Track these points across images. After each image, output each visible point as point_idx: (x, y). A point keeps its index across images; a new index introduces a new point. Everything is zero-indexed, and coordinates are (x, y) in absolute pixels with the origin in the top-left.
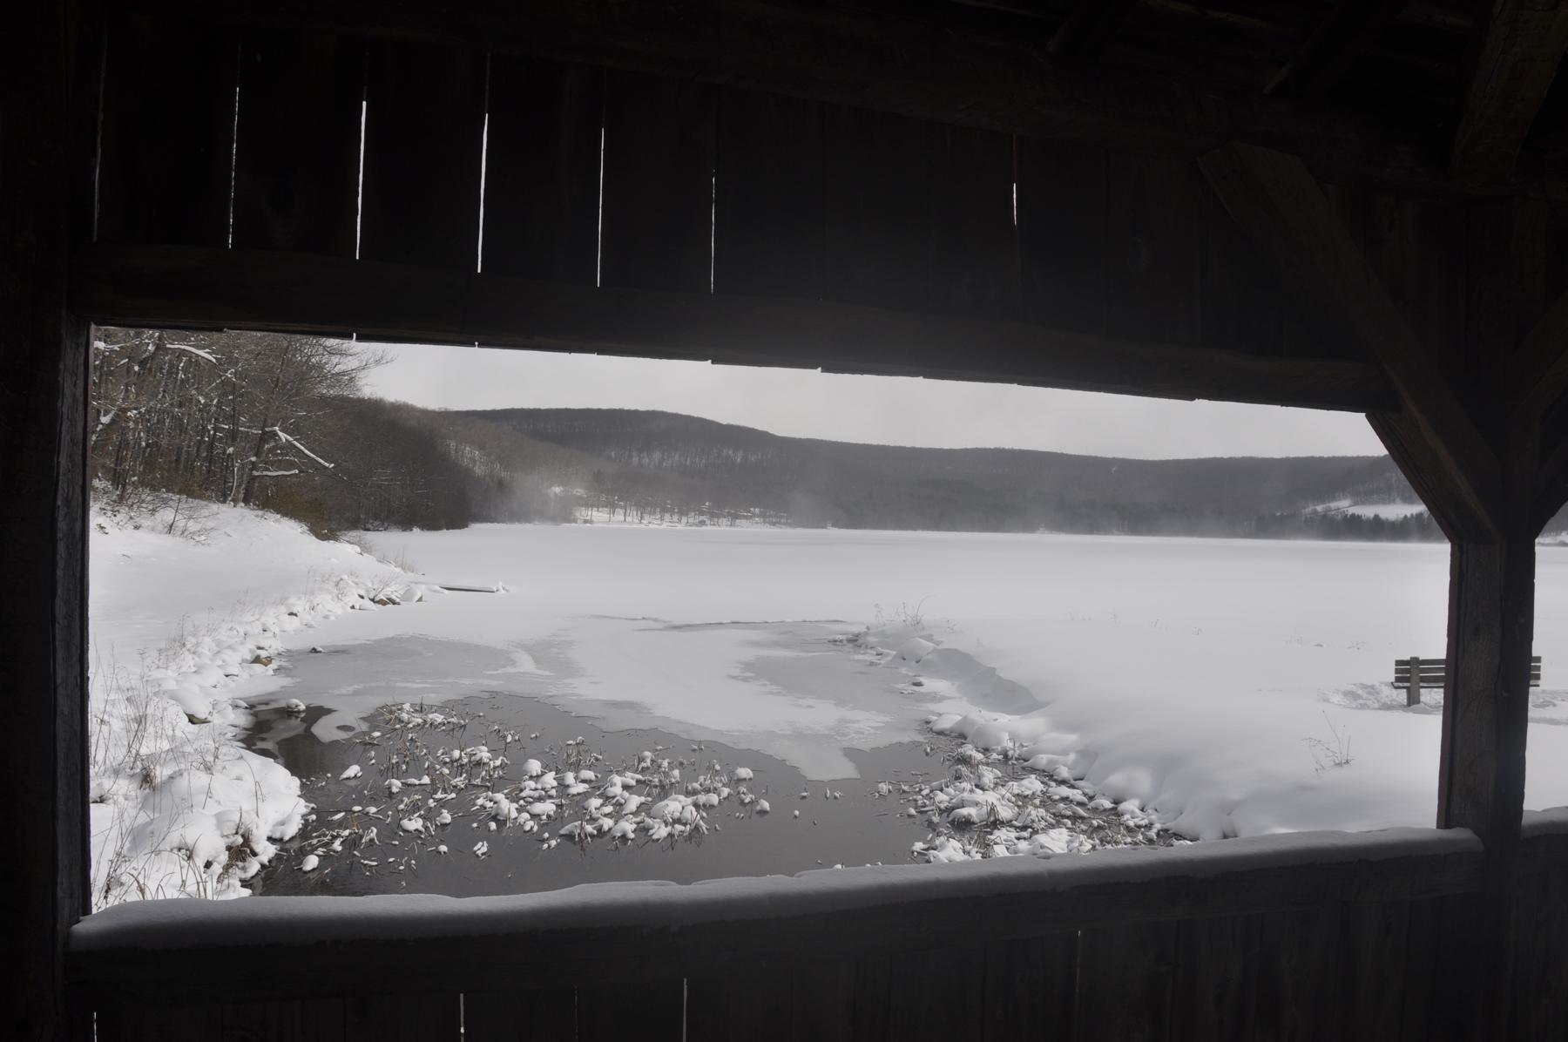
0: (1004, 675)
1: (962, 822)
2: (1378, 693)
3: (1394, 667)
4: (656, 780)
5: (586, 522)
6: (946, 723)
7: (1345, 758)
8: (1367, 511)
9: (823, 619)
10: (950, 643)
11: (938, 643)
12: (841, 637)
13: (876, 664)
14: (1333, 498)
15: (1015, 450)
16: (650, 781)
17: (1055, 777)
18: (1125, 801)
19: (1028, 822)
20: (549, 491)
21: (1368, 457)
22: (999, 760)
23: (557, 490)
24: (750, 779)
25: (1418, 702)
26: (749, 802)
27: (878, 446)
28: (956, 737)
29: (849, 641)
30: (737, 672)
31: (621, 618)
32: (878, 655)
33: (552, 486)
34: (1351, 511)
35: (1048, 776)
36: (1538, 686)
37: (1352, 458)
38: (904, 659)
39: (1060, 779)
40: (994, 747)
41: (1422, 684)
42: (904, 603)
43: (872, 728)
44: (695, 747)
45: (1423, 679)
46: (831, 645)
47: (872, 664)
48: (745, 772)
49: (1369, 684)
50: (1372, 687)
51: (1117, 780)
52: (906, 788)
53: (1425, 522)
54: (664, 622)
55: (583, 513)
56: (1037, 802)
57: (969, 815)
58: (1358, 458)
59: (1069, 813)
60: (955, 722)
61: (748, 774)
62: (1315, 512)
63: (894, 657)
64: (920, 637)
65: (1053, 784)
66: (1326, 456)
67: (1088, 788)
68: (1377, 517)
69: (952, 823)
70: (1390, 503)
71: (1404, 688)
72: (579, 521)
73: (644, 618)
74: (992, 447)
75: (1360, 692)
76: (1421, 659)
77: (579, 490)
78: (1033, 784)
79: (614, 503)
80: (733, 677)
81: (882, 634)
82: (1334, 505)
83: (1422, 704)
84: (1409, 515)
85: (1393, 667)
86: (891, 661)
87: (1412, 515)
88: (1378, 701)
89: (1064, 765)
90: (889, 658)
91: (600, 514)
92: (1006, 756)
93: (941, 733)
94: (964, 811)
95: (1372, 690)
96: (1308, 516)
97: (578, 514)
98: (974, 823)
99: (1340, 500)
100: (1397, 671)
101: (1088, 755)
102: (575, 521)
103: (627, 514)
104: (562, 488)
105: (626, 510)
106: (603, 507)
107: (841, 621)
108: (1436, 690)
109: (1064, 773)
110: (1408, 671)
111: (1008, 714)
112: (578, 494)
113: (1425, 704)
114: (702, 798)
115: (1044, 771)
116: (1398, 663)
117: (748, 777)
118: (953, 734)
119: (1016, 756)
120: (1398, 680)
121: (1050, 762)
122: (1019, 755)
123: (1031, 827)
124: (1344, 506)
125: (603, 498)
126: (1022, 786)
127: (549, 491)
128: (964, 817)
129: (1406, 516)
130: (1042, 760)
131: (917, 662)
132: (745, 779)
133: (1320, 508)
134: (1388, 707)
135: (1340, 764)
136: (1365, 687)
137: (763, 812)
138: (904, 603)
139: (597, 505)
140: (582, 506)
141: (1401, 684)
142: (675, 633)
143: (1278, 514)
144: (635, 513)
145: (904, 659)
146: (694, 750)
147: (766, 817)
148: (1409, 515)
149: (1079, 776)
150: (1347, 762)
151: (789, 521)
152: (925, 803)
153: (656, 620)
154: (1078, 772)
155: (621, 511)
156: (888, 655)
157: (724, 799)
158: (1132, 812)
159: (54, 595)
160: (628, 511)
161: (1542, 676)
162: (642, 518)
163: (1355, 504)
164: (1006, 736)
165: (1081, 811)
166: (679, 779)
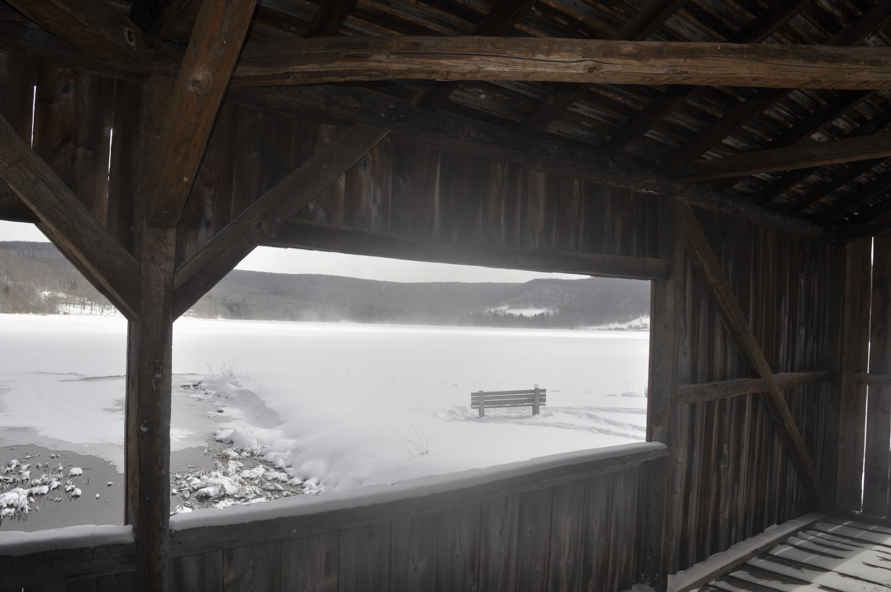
0: (268, 405)
1: (203, 496)
2: (466, 411)
3: (471, 397)
4: (12, 479)
5: (65, 313)
6: (222, 435)
7: (426, 450)
8: (517, 312)
9: (178, 373)
10: (246, 386)
11: (240, 386)
12: (189, 384)
13: (203, 400)
14: (499, 305)
15: (329, 276)
16: (7, 480)
17: (275, 466)
18: (309, 479)
19: (243, 495)
20: (41, 294)
21: (517, 283)
22: (247, 457)
23: (47, 293)
24: (80, 475)
25: (484, 416)
26: (70, 490)
27: (250, 272)
28: (228, 443)
29: (194, 386)
30: (111, 406)
31: (53, 374)
32: (206, 394)
33: (43, 291)
34: (508, 312)
35: (270, 465)
36: (545, 405)
37: (509, 284)
38: (219, 396)
39: (278, 467)
40: (245, 449)
41: (485, 406)
42: (224, 363)
43: (178, 439)
44: (53, 455)
45: (486, 403)
46: (182, 389)
47: (199, 399)
48: (77, 471)
49: (463, 406)
50: (464, 408)
51: (306, 467)
52: (178, 476)
53: (545, 318)
54: (81, 375)
55: (63, 308)
56: (257, 482)
57: (208, 492)
58: (512, 283)
59: (272, 488)
60: (228, 434)
61: (79, 471)
62: (490, 312)
63: (214, 395)
64: (231, 383)
65: (272, 470)
66: (496, 282)
67: (292, 472)
68: (521, 315)
69: (197, 497)
70: (528, 308)
71: (476, 408)
72: (61, 313)
73: (69, 374)
74: (316, 274)
75: (457, 411)
76: (484, 391)
77: (61, 294)
78: (260, 470)
79: (84, 302)
80: (106, 410)
81: (211, 381)
82: (500, 308)
83: (485, 417)
84: (537, 314)
85: (470, 397)
86: (212, 397)
87: (539, 314)
88: (464, 416)
89: (283, 458)
90: (211, 396)
91: (76, 309)
92: (252, 454)
93: (220, 441)
94: (205, 490)
95: (463, 409)
96: (486, 314)
97: (60, 309)
98: (211, 497)
99: (503, 306)
100: (472, 399)
101: (297, 451)
102: (58, 313)
103: (93, 309)
104: (50, 292)
105: (92, 306)
106: (77, 304)
107: (195, 374)
108: (498, 408)
109: (281, 463)
110: (478, 399)
111: (261, 428)
112: (61, 296)
113: (488, 417)
114: (35, 490)
115: (271, 462)
116: (473, 394)
117: (78, 474)
118: (227, 442)
119: (259, 453)
120: (473, 403)
121: (276, 457)
122: (261, 453)
123: (225, 494)
124: (505, 309)
125: (77, 299)
126: (252, 472)
127: (41, 294)
128: (205, 493)
129: (536, 315)
130: (270, 456)
131: (227, 398)
132: (76, 475)
133: (492, 310)
134: (468, 419)
135: (423, 454)
136: (460, 407)
137: (77, 496)
138: (224, 363)
139: (74, 303)
140: (63, 304)
141: (475, 406)
142: (86, 383)
143: (471, 313)
144: (98, 308)
145: (219, 396)
146: (52, 457)
147: (79, 499)
148: (537, 314)
149: (289, 465)
150: (427, 452)
151: (195, 315)
152: (185, 486)
153: (76, 374)
154: (289, 463)
155: (89, 307)
156: (211, 394)
157: (54, 489)
158: (311, 486)
159: (745, 405)
160: (94, 307)
161: (470, 395)
162: (102, 311)
163: (510, 308)
164: (255, 442)
165: (280, 487)
166: (28, 477)
